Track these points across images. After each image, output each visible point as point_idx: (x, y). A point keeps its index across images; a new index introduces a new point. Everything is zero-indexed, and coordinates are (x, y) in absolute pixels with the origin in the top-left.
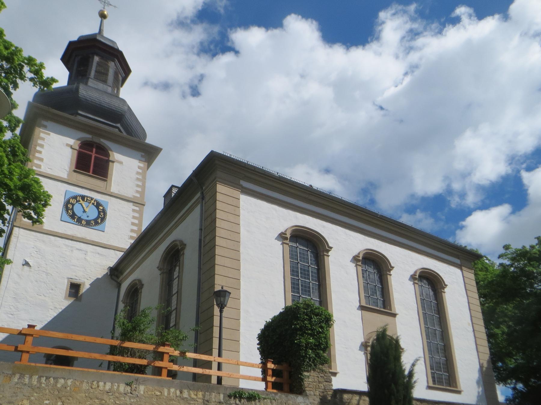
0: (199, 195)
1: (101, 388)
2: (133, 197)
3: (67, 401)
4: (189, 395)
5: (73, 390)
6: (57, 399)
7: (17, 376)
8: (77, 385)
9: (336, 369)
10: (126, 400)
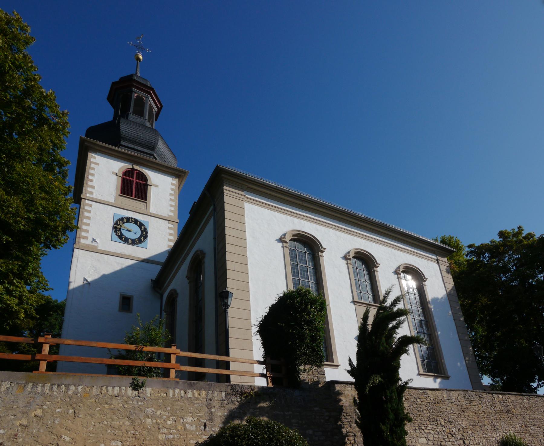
0: (212, 207)
1: (110, 393)
2: (168, 216)
3: (79, 408)
4: (193, 394)
5: (83, 396)
6: (69, 406)
7: (30, 385)
8: (87, 391)
9: (338, 362)
10: (134, 404)
